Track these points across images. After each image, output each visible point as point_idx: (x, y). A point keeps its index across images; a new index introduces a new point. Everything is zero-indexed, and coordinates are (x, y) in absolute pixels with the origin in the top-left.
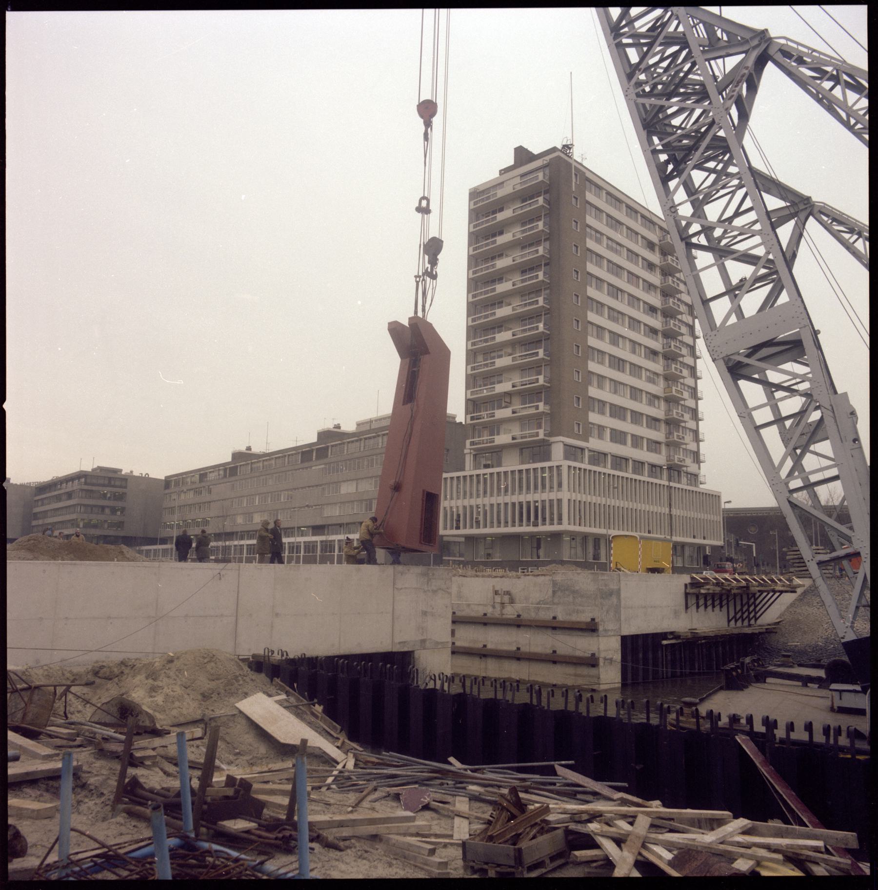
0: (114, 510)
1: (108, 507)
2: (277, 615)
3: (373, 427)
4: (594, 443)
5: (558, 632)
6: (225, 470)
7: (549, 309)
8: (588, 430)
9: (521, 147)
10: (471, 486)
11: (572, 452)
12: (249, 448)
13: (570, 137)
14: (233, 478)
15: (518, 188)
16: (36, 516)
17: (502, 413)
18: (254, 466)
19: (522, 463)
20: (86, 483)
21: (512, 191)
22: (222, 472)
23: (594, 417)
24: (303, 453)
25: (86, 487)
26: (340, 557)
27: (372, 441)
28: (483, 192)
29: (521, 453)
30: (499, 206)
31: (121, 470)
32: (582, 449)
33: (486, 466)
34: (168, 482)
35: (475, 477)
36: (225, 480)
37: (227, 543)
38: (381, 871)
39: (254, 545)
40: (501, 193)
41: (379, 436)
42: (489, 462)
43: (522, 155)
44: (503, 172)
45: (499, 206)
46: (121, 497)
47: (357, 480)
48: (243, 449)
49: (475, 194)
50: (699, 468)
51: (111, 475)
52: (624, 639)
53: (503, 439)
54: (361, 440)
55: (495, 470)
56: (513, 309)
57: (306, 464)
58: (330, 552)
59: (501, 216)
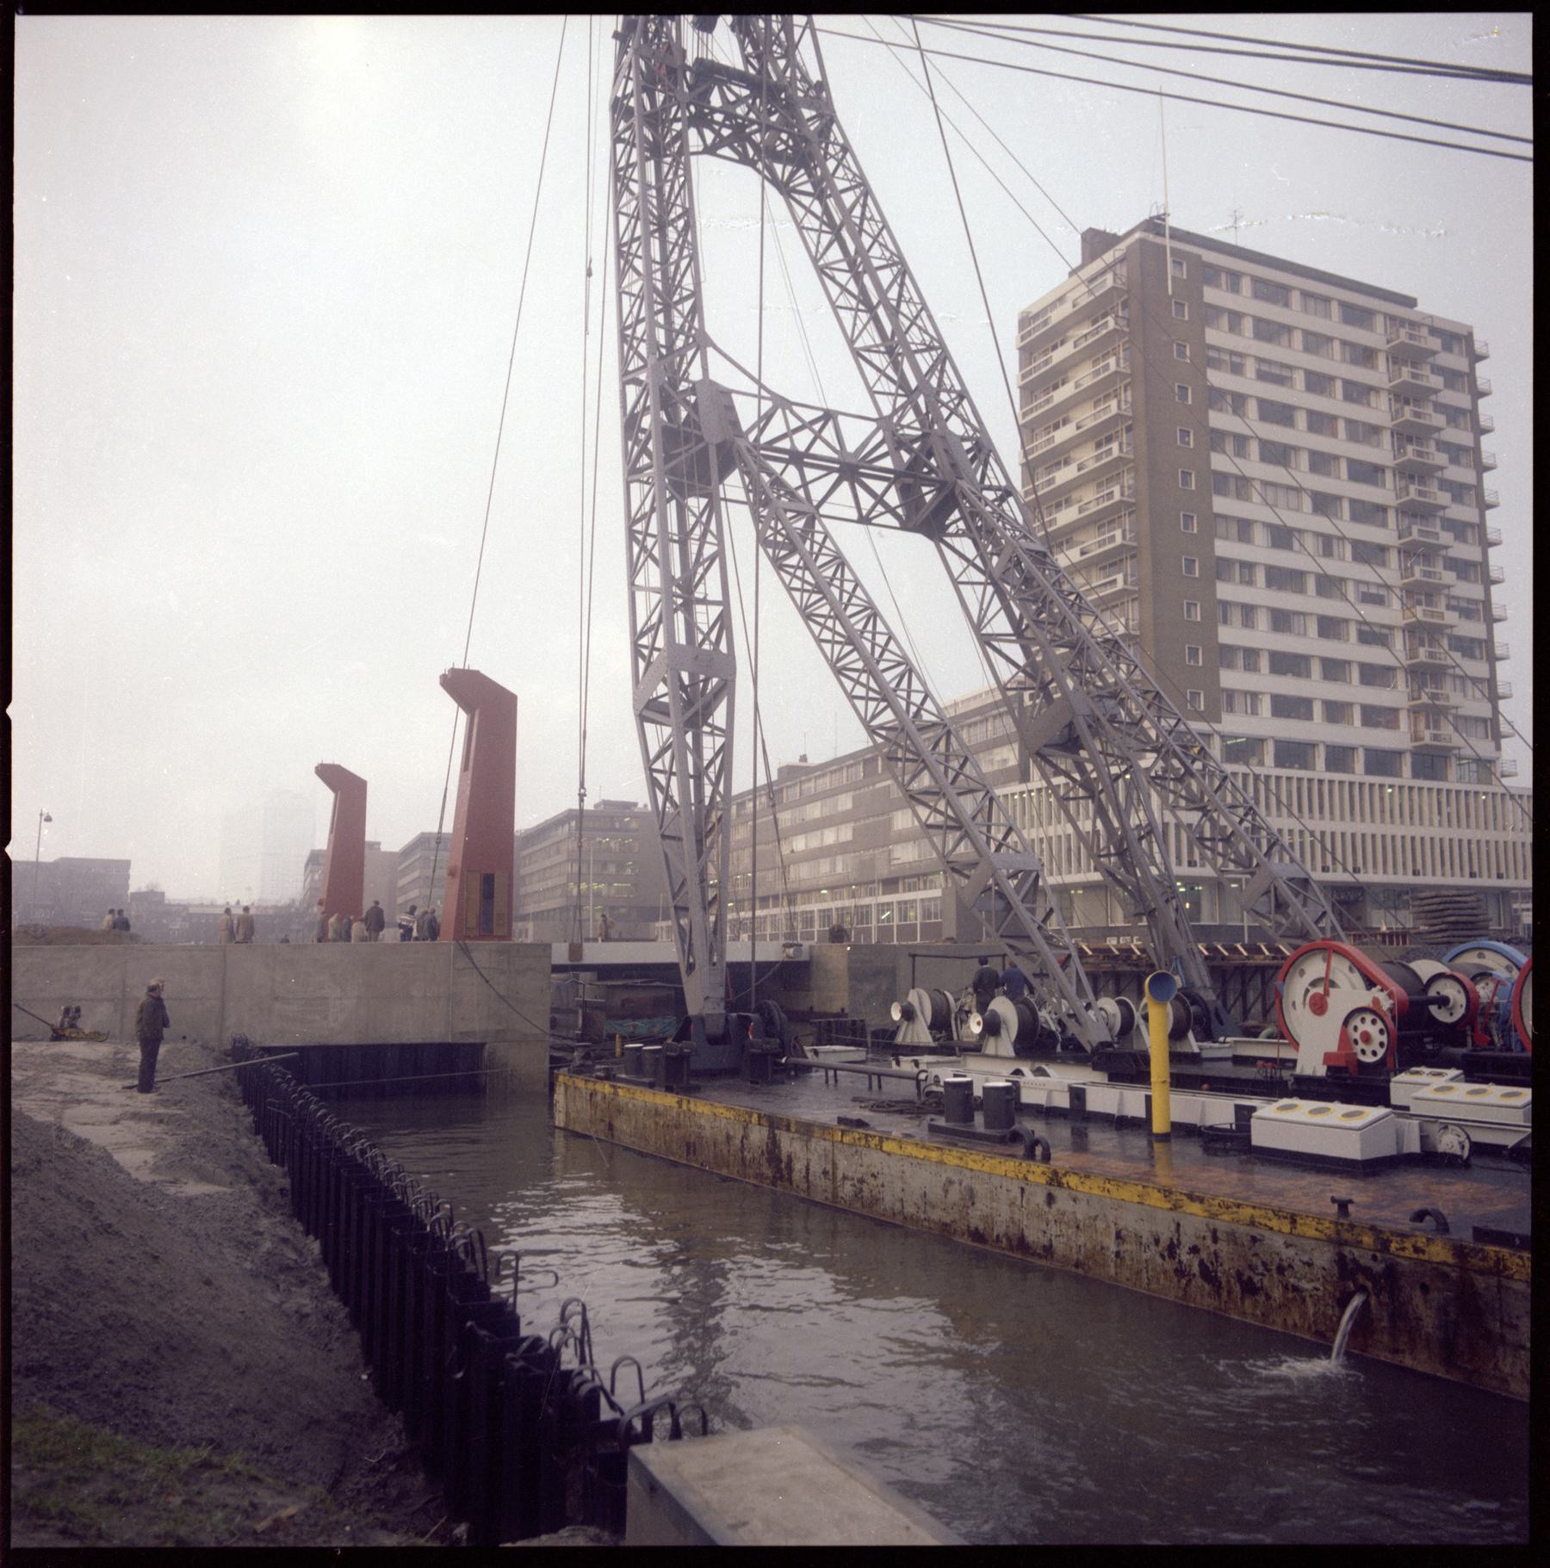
4: (1235, 724)
9: (1091, 230)
12: (804, 758)
23: (1231, 679)
24: (866, 762)
28: (1037, 316)
30: (1055, 337)
31: (635, 804)
38: (1159, 1543)
39: (935, 899)
40: (1056, 316)
43: (1096, 242)
44: (1073, 272)
45: (1055, 337)
48: (794, 760)
49: (1025, 321)
50: (1498, 748)
54: (987, 720)
59: (1058, 355)
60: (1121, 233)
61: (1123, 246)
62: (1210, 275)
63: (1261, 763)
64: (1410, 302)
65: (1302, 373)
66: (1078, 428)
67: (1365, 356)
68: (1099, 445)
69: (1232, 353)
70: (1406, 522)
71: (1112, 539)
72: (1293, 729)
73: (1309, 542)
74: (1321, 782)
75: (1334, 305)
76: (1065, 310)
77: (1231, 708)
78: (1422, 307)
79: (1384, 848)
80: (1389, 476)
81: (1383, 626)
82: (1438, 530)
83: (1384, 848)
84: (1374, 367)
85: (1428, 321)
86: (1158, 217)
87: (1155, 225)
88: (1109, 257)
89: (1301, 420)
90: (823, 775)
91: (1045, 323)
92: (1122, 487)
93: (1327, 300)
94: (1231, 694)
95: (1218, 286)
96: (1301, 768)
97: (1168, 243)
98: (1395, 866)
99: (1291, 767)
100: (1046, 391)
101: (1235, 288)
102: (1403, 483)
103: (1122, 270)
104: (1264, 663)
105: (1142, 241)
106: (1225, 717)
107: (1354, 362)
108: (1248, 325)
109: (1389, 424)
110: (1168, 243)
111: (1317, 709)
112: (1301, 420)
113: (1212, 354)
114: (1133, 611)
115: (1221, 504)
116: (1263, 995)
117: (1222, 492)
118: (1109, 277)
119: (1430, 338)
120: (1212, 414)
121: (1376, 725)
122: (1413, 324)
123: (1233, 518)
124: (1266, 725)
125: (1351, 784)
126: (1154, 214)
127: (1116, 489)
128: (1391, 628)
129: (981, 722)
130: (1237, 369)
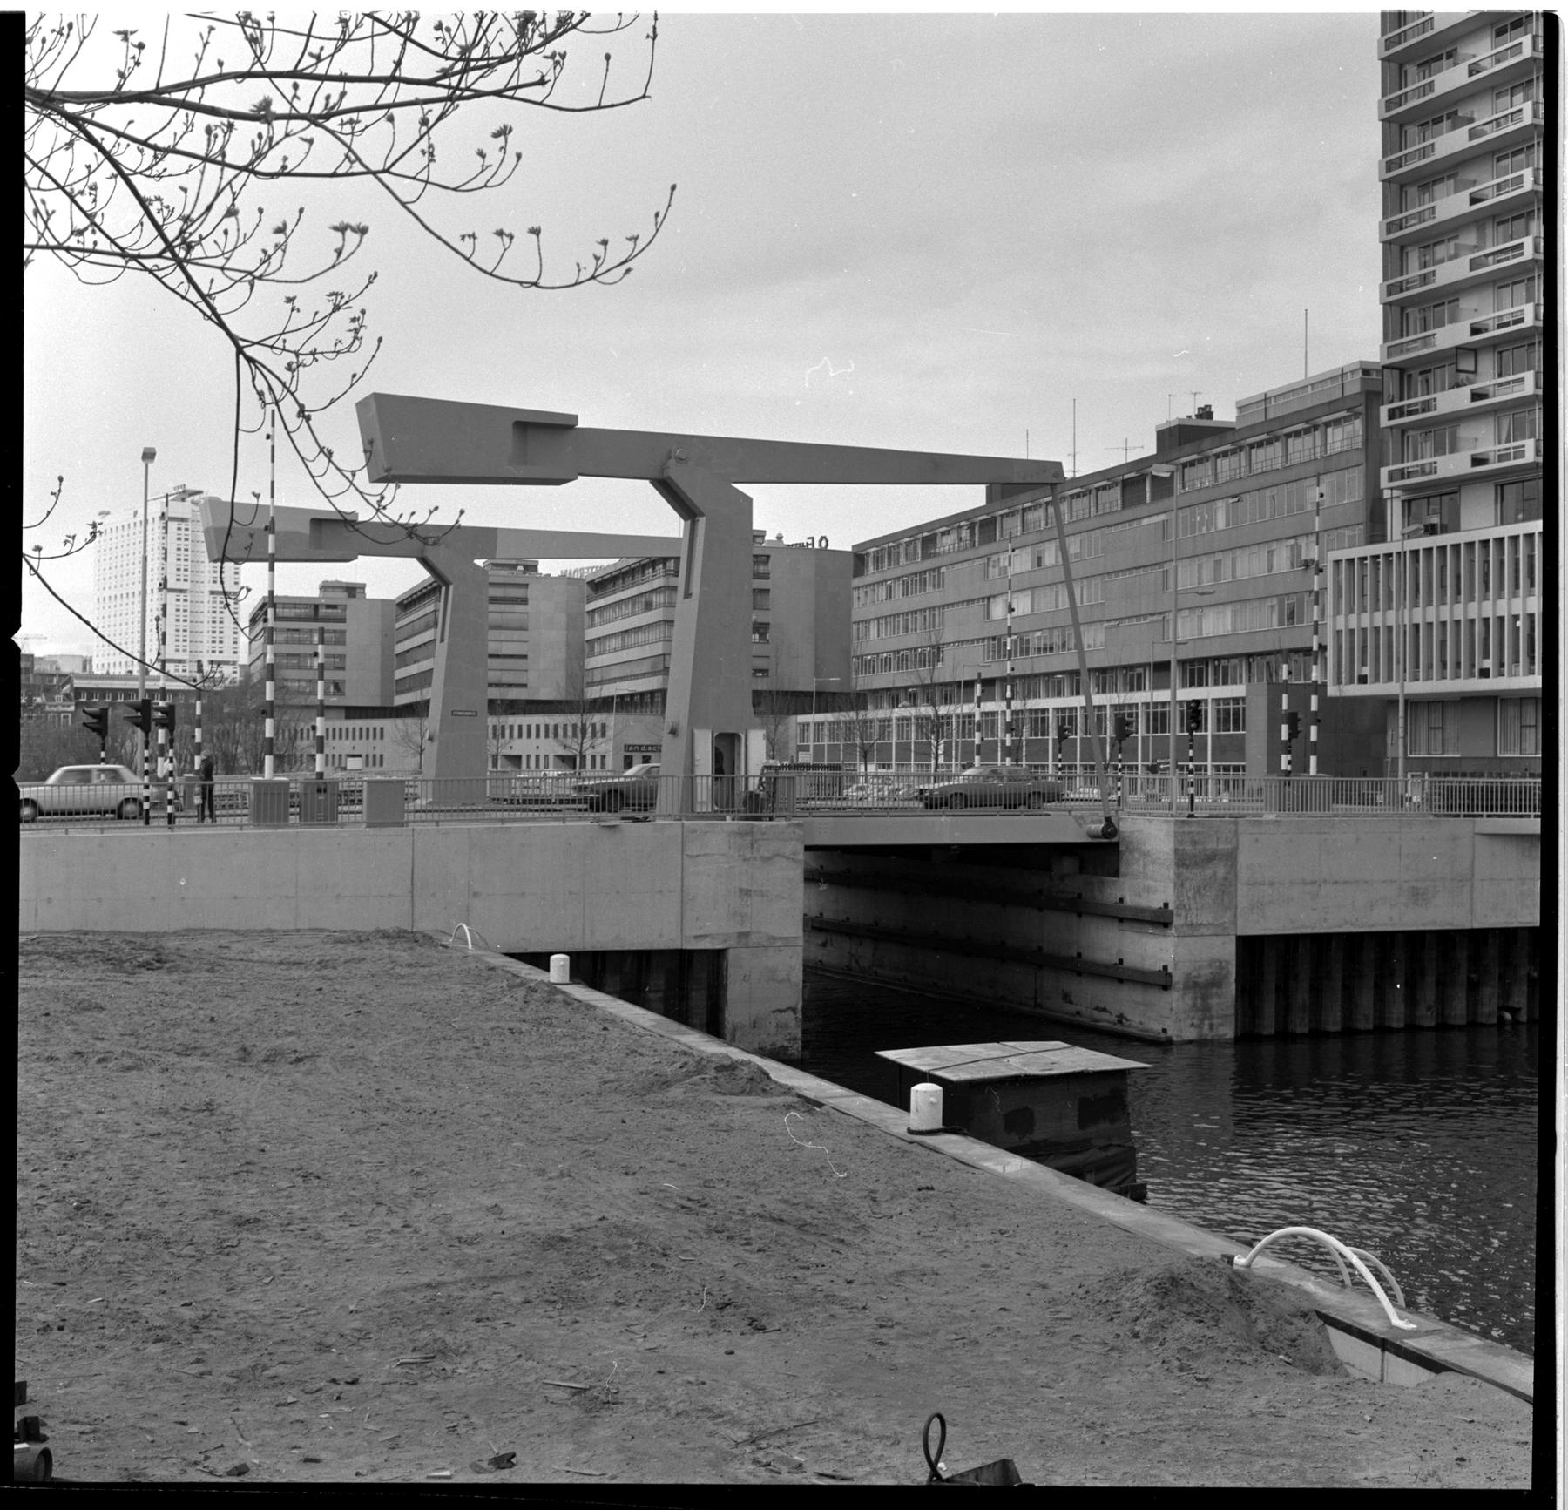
2: (476, 895)
3: (1271, 416)
5: (1125, 926)
6: (971, 527)
14: (1161, 505)
17: (1452, 400)
18: (1030, 516)
22: (965, 533)
24: (1126, 484)
29: (1501, 497)
33: (1431, 530)
34: (859, 558)
35: (1344, 564)
36: (970, 554)
37: (943, 710)
42: (1435, 520)
47: (1032, 588)
52: (1239, 938)
53: (1453, 465)
55: (1447, 539)
56: (1473, 135)
58: (1237, 728)
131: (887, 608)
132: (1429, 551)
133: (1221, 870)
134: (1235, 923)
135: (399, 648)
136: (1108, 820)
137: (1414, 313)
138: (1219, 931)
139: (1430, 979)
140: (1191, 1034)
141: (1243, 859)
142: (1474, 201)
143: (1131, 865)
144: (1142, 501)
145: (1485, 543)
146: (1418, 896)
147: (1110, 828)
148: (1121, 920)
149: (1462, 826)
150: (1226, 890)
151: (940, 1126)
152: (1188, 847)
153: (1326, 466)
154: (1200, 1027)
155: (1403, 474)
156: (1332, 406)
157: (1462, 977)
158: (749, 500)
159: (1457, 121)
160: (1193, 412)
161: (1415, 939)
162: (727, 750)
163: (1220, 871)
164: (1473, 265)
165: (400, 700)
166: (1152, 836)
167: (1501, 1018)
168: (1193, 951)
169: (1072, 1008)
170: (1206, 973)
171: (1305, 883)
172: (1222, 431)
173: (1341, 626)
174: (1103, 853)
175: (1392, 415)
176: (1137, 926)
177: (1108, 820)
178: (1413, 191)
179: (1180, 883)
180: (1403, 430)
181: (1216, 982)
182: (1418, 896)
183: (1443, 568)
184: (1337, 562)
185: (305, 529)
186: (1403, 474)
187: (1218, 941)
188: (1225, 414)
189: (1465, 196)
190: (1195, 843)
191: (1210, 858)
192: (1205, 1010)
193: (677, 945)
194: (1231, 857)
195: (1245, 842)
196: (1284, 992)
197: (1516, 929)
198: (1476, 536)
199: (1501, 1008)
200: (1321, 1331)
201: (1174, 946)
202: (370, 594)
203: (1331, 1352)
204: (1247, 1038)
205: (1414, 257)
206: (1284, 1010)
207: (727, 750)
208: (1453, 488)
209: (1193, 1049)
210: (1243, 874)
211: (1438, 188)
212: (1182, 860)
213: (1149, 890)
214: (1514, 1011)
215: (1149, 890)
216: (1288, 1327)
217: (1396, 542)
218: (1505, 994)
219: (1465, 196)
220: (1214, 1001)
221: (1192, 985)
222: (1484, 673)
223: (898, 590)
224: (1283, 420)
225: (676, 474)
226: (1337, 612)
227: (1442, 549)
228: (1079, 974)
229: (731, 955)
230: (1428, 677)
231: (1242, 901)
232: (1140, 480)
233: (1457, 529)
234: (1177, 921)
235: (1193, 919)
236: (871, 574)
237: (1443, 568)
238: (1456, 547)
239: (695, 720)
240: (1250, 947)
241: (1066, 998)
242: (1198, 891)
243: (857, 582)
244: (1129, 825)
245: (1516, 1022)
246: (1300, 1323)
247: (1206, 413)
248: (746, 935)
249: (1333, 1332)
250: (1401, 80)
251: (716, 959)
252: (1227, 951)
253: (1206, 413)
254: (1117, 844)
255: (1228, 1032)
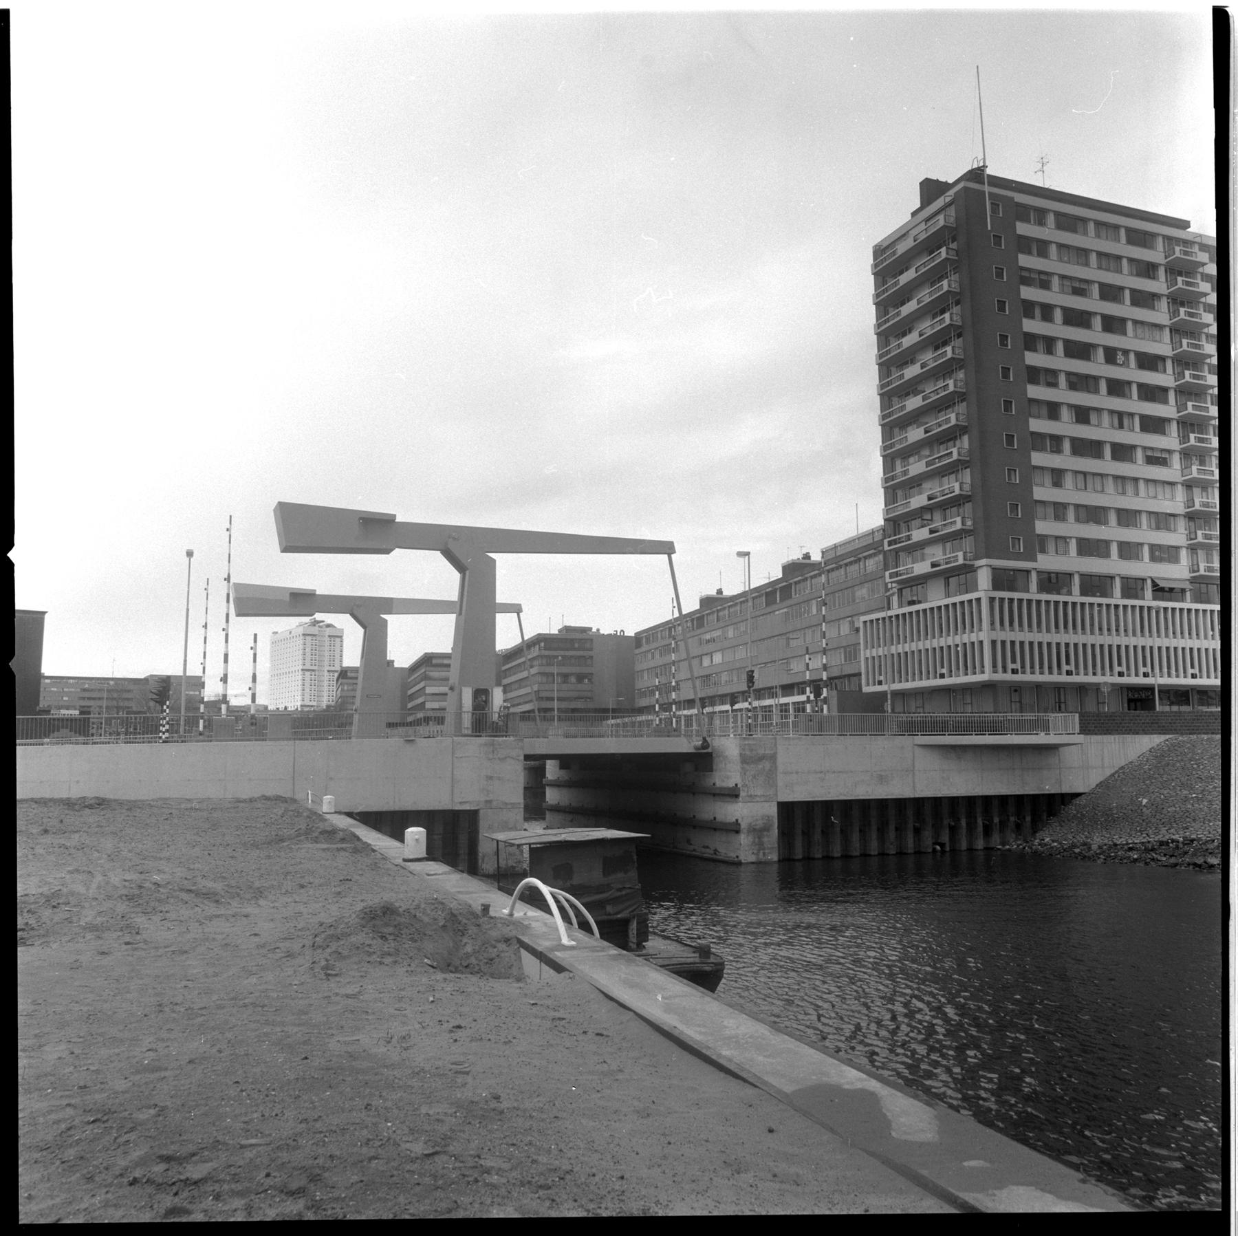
0: (580, 678)
1: (572, 674)
4: (1048, 562)
6: (692, 621)
7: (964, 394)
8: (1042, 543)
10: (905, 630)
11: (1002, 580)
12: (720, 592)
13: (981, 157)
15: (923, 236)
16: (412, 697)
18: (721, 614)
19: (948, 596)
20: (545, 649)
21: (913, 244)
22: (689, 624)
24: (767, 594)
25: (547, 653)
26: (795, 725)
27: (856, 567)
28: (887, 247)
29: (947, 584)
30: (902, 264)
32: (1028, 572)
33: (912, 603)
34: (639, 639)
40: (902, 248)
41: (841, 567)
43: (931, 189)
44: (914, 214)
45: (902, 264)
46: (583, 660)
48: (713, 592)
49: (879, 251)
51: (578, 636)
54: (860, 559)
56: (924, 399)
57: (769, 609)
60: (951, 181)
61: (952, 192)
62: (1023, 213)
63: (1070, 593)
64: (1184, 225)
65: (1097, 285)
66: (921, 335)
67: (1148, 270)
68: (937, 348)
69: (1040, 272)
70: (1183, 399)
71: (948, 420)
72: (1095, 566)
73: (1106, 417)
74: (1117, 606)
75: (1125, 262)
76: (908, 244)
77: (1043, 550)
78: (1193, 229)
79: (1168, 658)
80: (1169, 364)
81: (1162, 450)
82: (1201, 311)
83: (1168, 658)
84: (1166, 402)
85: (1198, 240)
86: (979, 169)
87: (976, 174)
88: (939, 203)
89: (1097, 322)
90: (735, 605)
91: (894, 253)
92: (955, 380)
93: (1117, 227)
94: (1043, 539)
95: (1028, 221)
96: (1101, 596)
97: (987, 189)
98: (1177, 670)
99: (1094, 595)
100: (895, 276)
101: (1057, 483)
102: (1180, 369)
103: (952, 211)
104: (1067, 446)
105: (965, 188)
106: (1040, 557)
107: (1139, 274)
108: (1058, 315)
109: (1163, 261)
110: (987, 189)
111: (1114, 549)
112: (1097, 322)
113: (1025, 274)
114: (962, 408)
115: (1038, 458)
116: (1040, 216)
117: (1042, 449)
118: (941, 217)
119: (1200, 254)
120: (1021, 256)
121: (1161, 560)
122: (1186, 243)
123: (1050, 502)
124: (1072, 562)
125: (1141, 608)
126: (975, 166)
127: (951, 382)
128: (1170, 452)
129: (855, 562)
130: (1045, 285)
131: (652, 664)
132: (911, 613)
133: (767, 765)
134: (776, 795)
135: (410, 692)
136: (704, 739)
137: (899, 493)
138: (767, 799)
139: (892, 827)
140: (753, 858)
141: (780, 759)
142: (926, 432)
143: (718, 764)
144: (775, 602)
145: (939, 608)
146: (882, 779)
147: (705, 744)
148: (714, 795)
149: (907, 741)
150: (770, 777)
151: (424, 855)
152: (748, 753)
153: (866, 579)
154: (757, 854)
155: (897, 574)
156: (867, 548)
157: (910, 825)
158: (494, 561)
159: (916, 393)
160: (801, 557)
161: (882, 804)
162: (481, 696)
163: (777, 769)
164: (928, 464)
165: (410, 719)
166: (729, 746)
167: (934, 849)
168: (752, 810)
169: (692, 847)
170: (760, 823)
171: (816, 772)
172: (815, 566)
173: (868, 655)
174: (703, 759)
175: (890, 544)
176: (728, 799)
177: (704, 739)
178: (896, 430)
179: (744, 772)
180: (897, 551)
181: (766, 828)
182: (882, 779)
183: (919, 622)
184: (865, 622)
185: (287, 598)
186: (897, 574)
187: (767, 805)
188: (816, 557)
189: (922, 429)
190: (752, 750)
191: (761, 758)
192: (761, 845)
193: (449, 807)
194: (773, 758)
195: (780, 749)
196: (807, 834)
197: (940, 798)
198: (934, 604)
199: (935, 844)
200: (517, 953)
201: (748, 811)
202: (396, 665)
203: (520, 968)
204: (786, 860)
205: (898, 462)
206: (808, 844)
207: (481, 696)
208: (923, 579)
209: (753, 866)
210: (780, 768)
211: (910, 428)
212: (745, 760)
213: (728, 778)
214: (942, 845)
215: (728, 778)
216: (490, 950)
217: (896, 611)
218: (937, 834)
219: (922, 429)
220: (765, 839)
221: (752, 830)
222: (942, 676)
223: (657, 656)
224: (843, 557)
225: (452, 546)
226: (866, 648)
227: (918, 612)
228: (694, 827)
229: (481, 812)
230: (914, 680)
231: (780, 784)
232: (774, 592)
233: (926, 601)
234: (742, 794)
235: (752, 792)
236: (645, 648)
237: (919, 622)
238: (925, 611)
239: (463, 682)
240: (787, 810)
241: (689, 842)
242: (754, 777)
243: (637, 651)
244: (717, 743)
245: (943, 852)
246: (502, 946)
247: (807, 556)
248: (490, 802)
249: (523, 952)
250: (889, 374)
251: (473, 816)
252: (773, 810)
253: (807, 556)
254: (710, 754)
255: (774, 857)
